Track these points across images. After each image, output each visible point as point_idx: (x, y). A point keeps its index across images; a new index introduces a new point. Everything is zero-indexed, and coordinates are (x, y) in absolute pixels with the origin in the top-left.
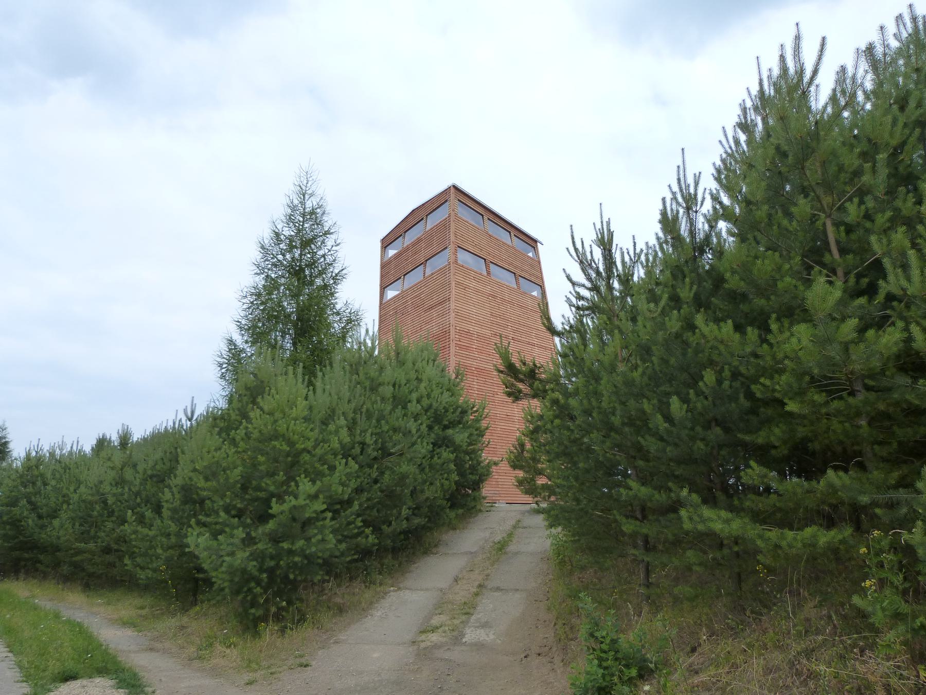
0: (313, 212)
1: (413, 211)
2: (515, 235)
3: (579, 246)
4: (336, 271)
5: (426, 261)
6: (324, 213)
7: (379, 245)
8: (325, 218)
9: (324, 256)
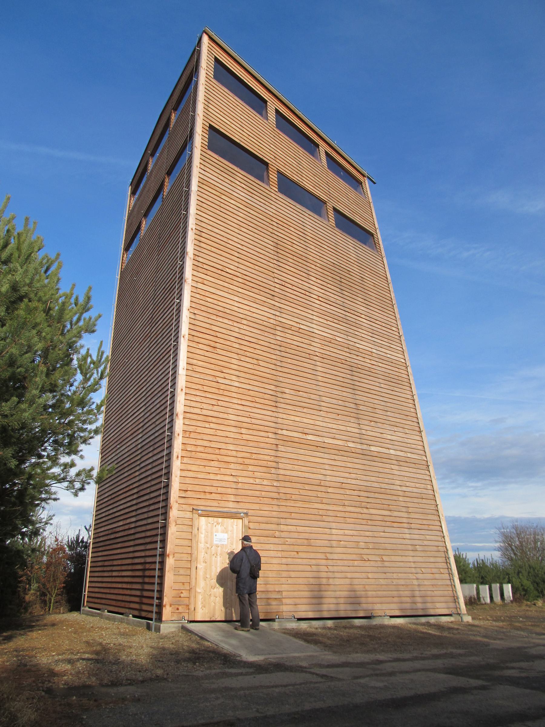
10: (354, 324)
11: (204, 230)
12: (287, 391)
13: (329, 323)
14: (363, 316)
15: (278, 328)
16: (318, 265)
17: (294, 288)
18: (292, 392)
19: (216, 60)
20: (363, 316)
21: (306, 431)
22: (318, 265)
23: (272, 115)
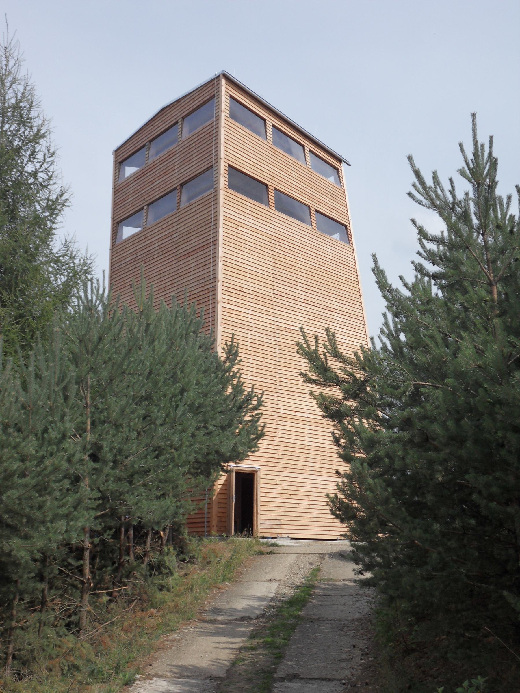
0: (16, 107)
1: (163, 110)
2: (310, 151)
3: (429, 182)
4: (53, 197)
5: (182, 185)
6: (31, 107)
7: (111, 159)
8: (33, 114)
9: (34, 174)
10: (329, 319)
11: (228, 260)
12: (283, 380)
13: (311, 321)
14: (336, 311)
15: (277, 331)
16: (304, 271)
17: (287, 296)
18: (287, 381)
19: (231, 97)
20: (336, 311)
21: (296, 410)
22: (304, 271)
23: (270, 129)
